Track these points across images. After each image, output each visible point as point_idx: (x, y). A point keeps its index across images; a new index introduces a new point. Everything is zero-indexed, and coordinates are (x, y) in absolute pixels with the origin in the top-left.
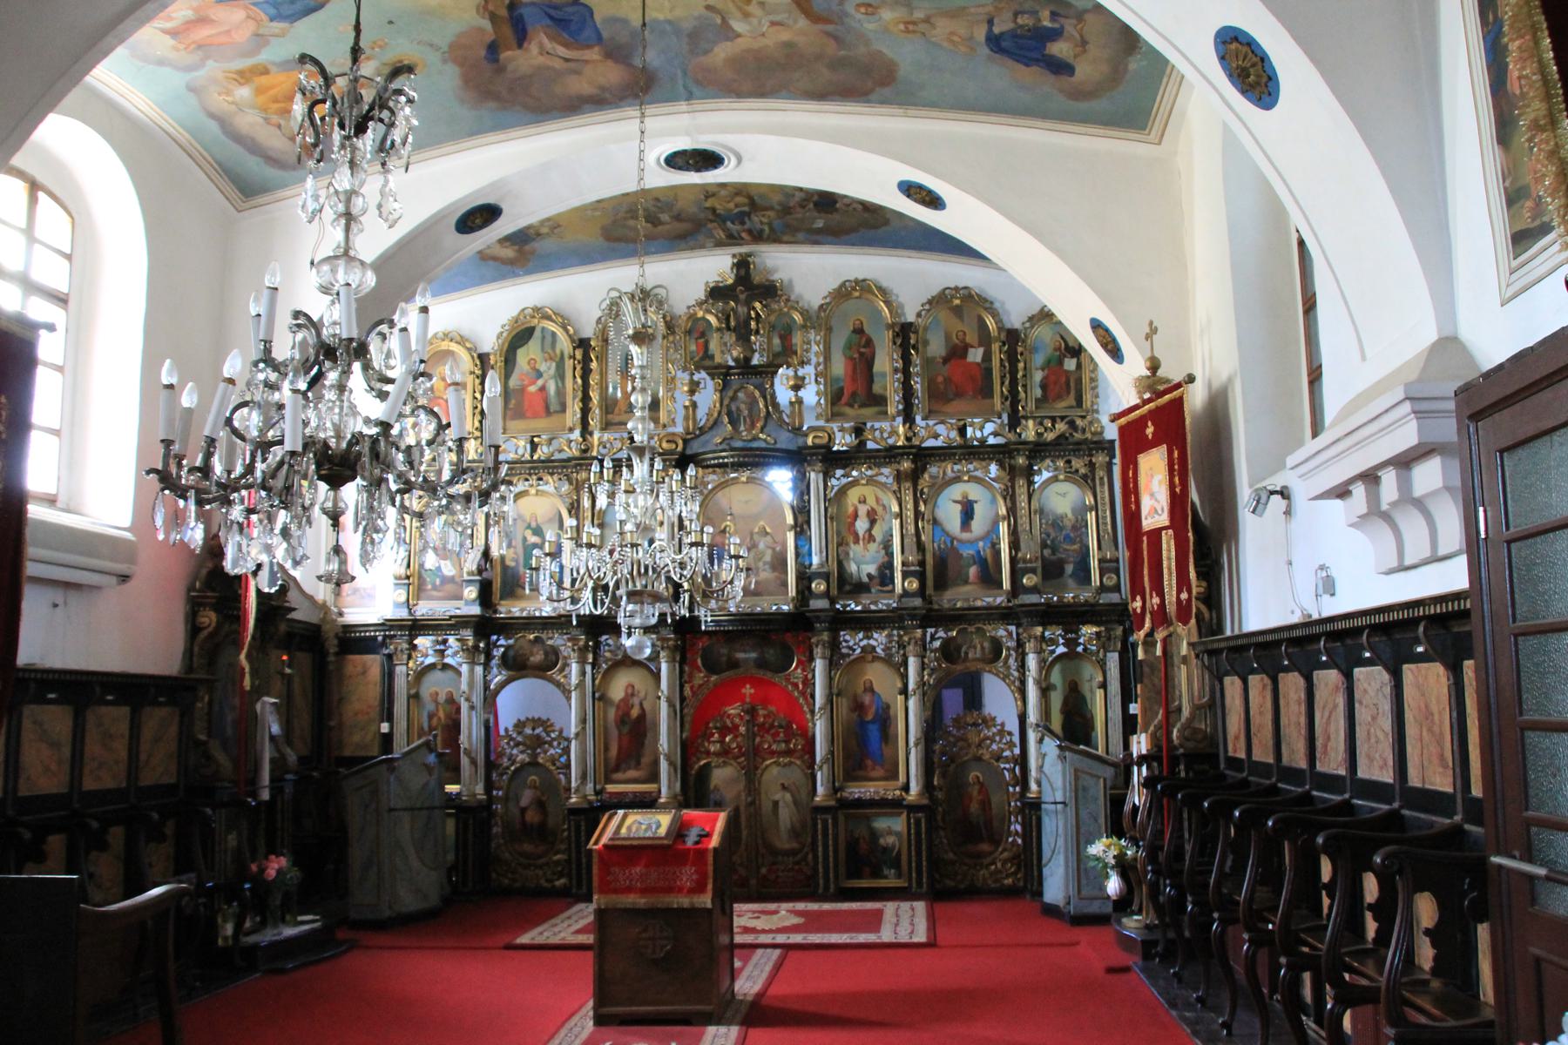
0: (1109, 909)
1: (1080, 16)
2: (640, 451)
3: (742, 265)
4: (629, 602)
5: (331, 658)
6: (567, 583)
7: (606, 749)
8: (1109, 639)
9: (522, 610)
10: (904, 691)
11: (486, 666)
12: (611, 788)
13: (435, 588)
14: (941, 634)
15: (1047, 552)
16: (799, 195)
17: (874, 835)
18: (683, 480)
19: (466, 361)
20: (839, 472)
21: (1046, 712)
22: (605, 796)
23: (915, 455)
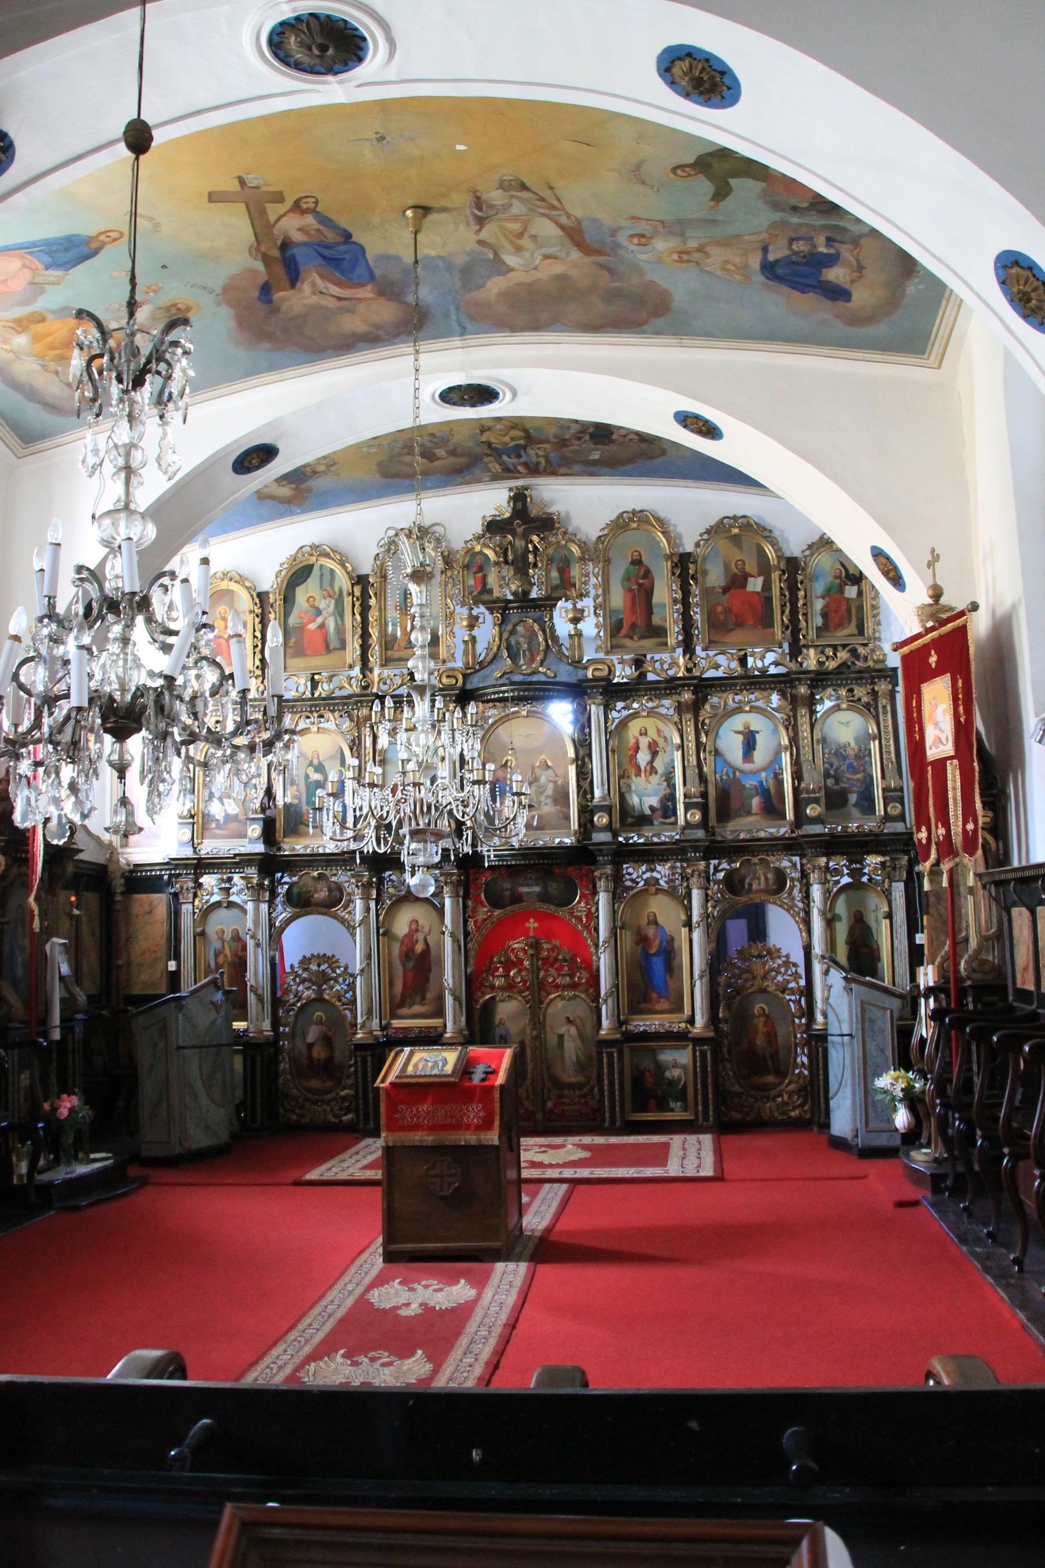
0: (897, 1141)
1: (856, 242)
2: (421, 690)
3: (519, 498)
4: (412, 840)
5: (118, 898)
6: (350, 823)
7: (391, 984)
8: (894, 869)
9: (306, 847)
10: (688, 924)
11: (271, 903)
12: (396, 1023)
13: (219, 826)
14: (725, 865)
15: (830, 782)
16: (575, 428)
17: (660, 1068)
18: (465, 715)
19: (245, 601)
20: (620, 705)
21: (831, 943)
22: (390, 1032)
23: (696, 686)
